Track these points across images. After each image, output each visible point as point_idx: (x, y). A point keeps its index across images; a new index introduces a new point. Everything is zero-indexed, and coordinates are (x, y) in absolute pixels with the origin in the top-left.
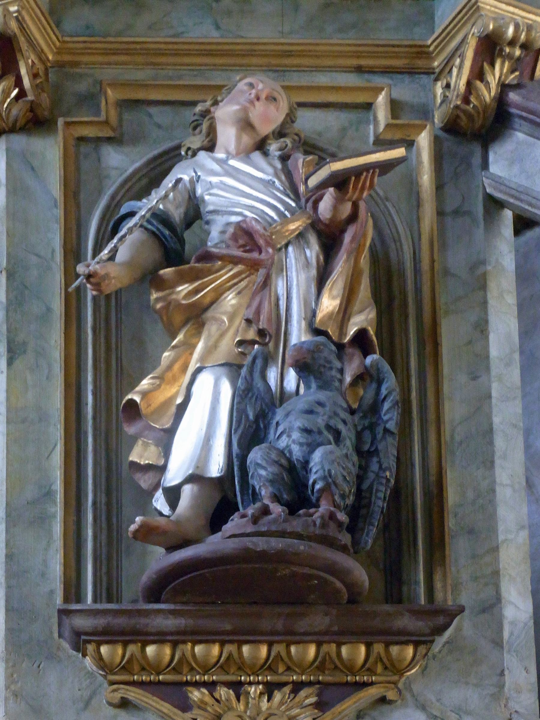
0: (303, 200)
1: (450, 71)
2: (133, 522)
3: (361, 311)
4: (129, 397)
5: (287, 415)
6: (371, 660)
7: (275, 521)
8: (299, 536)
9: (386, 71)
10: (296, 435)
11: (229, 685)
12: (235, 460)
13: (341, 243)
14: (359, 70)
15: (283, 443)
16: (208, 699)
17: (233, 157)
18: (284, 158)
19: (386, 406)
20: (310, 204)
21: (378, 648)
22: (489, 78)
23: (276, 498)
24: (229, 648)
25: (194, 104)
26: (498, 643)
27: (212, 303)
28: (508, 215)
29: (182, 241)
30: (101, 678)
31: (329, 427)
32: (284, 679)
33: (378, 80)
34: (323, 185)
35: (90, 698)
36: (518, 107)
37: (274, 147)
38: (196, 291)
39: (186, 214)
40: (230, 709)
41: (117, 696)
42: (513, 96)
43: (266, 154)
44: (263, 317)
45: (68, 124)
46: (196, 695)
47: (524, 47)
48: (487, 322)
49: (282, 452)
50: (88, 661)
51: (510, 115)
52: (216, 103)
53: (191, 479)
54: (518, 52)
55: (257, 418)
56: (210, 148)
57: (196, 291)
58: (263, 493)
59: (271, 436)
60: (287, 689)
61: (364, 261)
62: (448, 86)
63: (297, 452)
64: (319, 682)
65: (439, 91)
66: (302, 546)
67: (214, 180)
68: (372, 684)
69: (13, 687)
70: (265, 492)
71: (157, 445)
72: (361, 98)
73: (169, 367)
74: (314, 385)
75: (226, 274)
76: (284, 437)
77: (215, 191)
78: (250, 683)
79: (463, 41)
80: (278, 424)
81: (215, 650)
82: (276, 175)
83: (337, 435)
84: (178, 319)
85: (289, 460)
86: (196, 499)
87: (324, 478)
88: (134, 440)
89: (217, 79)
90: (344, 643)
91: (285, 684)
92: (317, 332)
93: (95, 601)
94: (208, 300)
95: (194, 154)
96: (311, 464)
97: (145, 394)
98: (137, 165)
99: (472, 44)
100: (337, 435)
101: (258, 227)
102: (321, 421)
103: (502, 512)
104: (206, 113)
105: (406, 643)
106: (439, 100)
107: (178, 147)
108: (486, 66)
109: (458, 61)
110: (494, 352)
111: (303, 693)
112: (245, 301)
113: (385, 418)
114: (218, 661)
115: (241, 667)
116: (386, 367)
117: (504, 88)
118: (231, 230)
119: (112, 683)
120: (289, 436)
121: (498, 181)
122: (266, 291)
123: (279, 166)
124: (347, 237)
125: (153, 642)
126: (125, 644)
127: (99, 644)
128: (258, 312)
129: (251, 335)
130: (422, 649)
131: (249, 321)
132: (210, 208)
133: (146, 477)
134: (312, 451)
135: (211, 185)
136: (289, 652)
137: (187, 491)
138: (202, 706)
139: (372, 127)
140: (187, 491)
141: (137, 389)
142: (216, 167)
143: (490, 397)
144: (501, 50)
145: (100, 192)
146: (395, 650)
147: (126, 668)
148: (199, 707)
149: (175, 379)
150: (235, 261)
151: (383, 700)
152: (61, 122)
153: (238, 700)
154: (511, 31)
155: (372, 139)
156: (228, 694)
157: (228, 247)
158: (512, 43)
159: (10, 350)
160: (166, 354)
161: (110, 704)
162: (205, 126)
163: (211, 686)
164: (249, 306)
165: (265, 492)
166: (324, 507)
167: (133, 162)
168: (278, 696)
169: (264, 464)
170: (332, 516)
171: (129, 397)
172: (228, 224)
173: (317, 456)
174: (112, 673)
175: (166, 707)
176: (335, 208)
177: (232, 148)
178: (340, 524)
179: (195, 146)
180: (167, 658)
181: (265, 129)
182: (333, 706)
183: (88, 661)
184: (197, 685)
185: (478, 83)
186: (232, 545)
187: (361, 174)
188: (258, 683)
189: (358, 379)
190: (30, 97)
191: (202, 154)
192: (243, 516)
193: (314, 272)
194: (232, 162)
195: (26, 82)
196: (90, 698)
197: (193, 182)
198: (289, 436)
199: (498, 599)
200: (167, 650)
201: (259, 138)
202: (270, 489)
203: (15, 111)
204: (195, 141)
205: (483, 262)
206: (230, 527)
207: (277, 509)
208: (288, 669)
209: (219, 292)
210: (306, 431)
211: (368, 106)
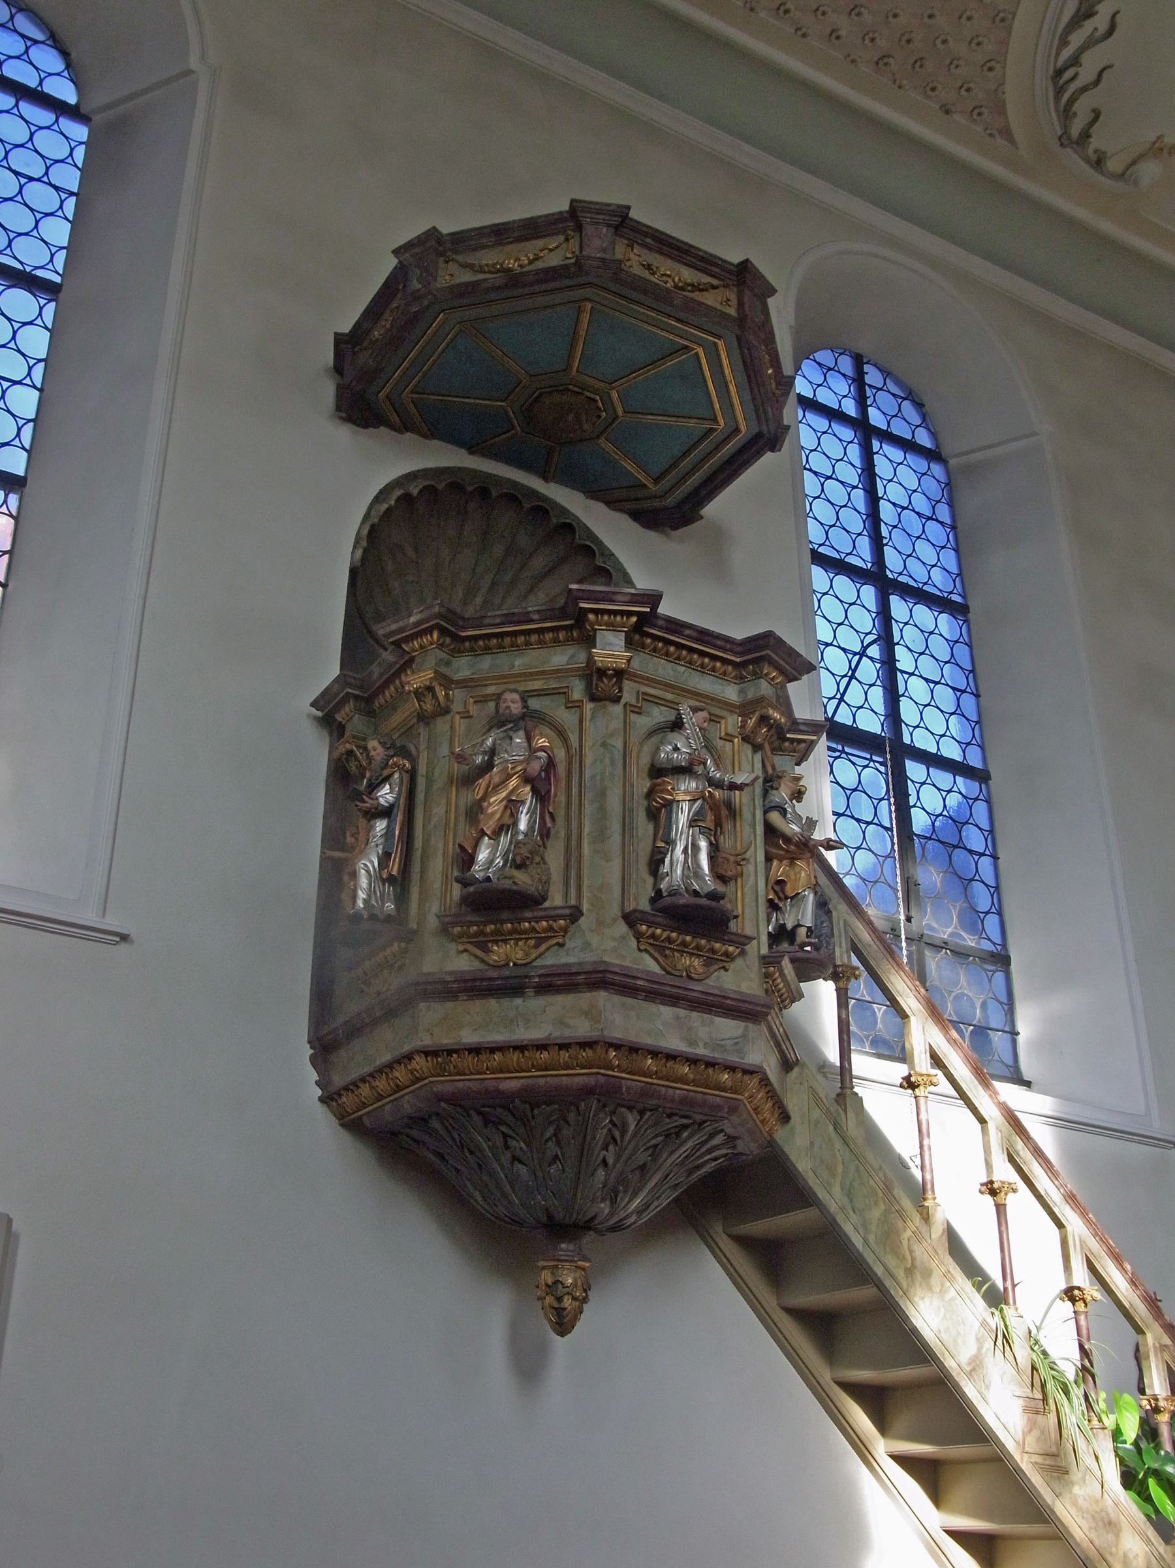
46: (667, 952)
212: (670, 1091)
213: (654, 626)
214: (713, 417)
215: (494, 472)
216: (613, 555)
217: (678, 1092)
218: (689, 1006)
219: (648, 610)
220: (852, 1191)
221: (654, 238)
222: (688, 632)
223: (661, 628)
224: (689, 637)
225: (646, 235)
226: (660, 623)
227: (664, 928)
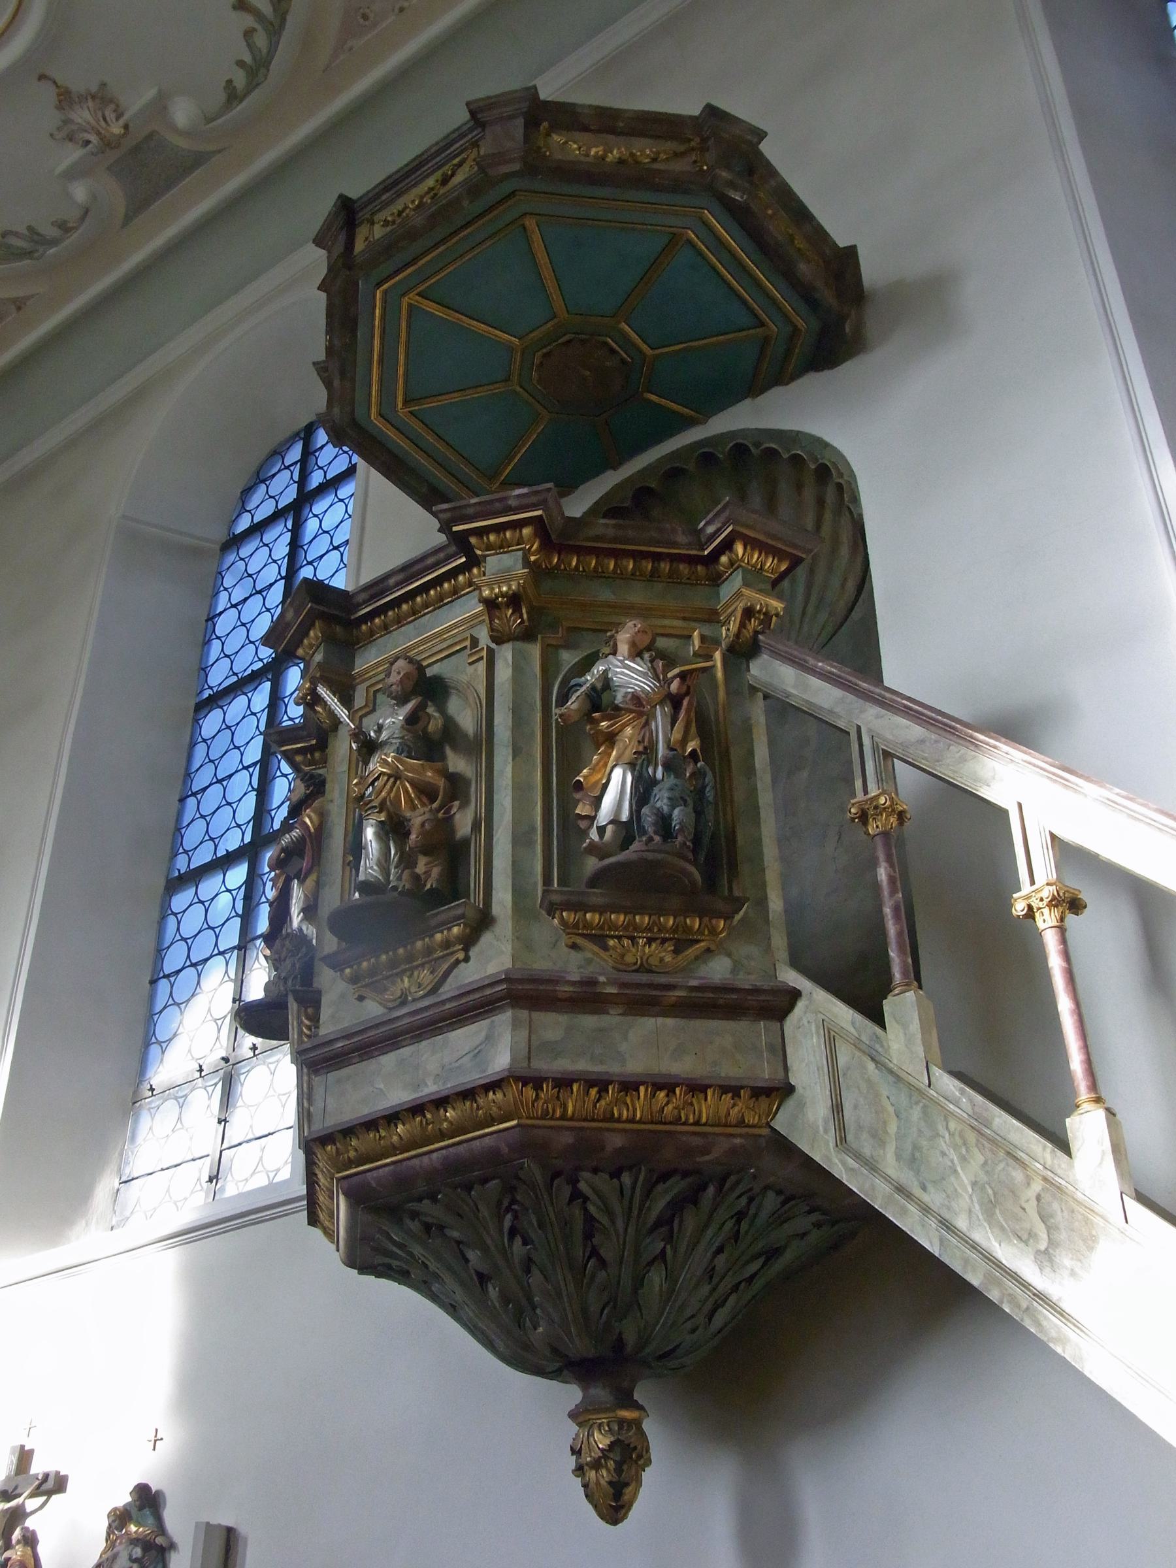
0: (662, 682)
1: (729, 623)
2: (585, 842)
3: (692, 740)
4: (577, 778)
5: (660, 791)
6: (703, 926)
7: (657, 844)
8: (668, 853)
9: (695, 620)
10: (665, 801)
11: (628, 938)
12: (634, 813)
13: (682, 705)
14: (684, 619)
15: (658, 804)
16: (618, 945)
17: (627, 660)
18: (652, 661)
19: (708, 789)
20: (666, 685)
21: (706, 920)
22: (749, 628)
23: (656, 833)
24: (630, 917)
25: (606, 631)
26: (767, 922)
27: (619, 732)
28: (760, 695)
29: (601, 698)
30: (562, 932)
31: (682, 798)
32: (657, 936)
33: (693, 624)
34: (675, 677)
35: (557, 941)
36: (764, 642)
37: (647, 656)
38: (612, 725)
39: (603, 685)
40: (629, 951)
41: (570, 942)
42: (760, 637)
43: (642, 659)
44: (646, 740)
45: (542, 638)
46: (611, 943)
47: (764, 614)
48: (753, 750)
49: (658, 809)
50: (556, 921)
51: (759, 645)
52: (617, 632)
53: (611, 822)
54: (762, 617)
55: (644, 792)
56: (614, 653)
57: (612, 725)
58: (650, 830)
59: (652, 801)
60: (658, 941)
61: (693, 714)
62: (728, 629)
63: (666, 809)
64: (675, 939)
65: (724, 632)
66: (670, 858)
67: (618, 670)
68: (703, 941)
69: (516, 934)
70: (650, 830)
71: (591, 805)
72: (686, 633)
73: (597, 764)
74: (672, 776)
75: (627, 718)
76: (659, 802)
77: (619, 676)
78: (640, 938)
79: (736, 608)
80: (655, 795)
81: (622, 917)
82: (649, 670)
83: (685, 802)
84: (601, 739)
85: (662, 814)
86: (614, 832)
87: (680, 823)
88: (578, 801)
89: (615, 619)
90: (688, 917)
91: (657, 939)
92: (672, 749)
93: (558, 886)
94: (617, 731)
95: (606, 657)
96: (674, 816)
97: (585, 777)
98: (577, 660)
99: (739, 614)
100: (685, 802)
101: (643, 696)
102: (677, 794)
103: (766, 850)
104: (612, 636)
105: (720, 917)
106: (724, 636)
107: (598, 651)
108: (747, 622)
109: (733, 618)
110: (757, 766)
111: (666, 945)
112: (637, 731)
113: (708, 795)
114: (623, 924)
115: (636, 928)
116: (707, 769)
117: (756, 633)
118: (629, 696)
119: (569, 934)
120: (662, 801)
121: (754, 677)
122: (647, 727)
123: (650, 665)
124: (685, 703)
125: (590, 911)
126: (576, 912)
127: (563, 910)
128: (643, 738)
129: (641, 749)
130: (728, 922)
131: (639, 742)
132: (617, 684)
133: (583, 822)
134: (674, 809)
135: (617, 673)
136: (660, 920)
137: (610, 828)
138: (614, 948)
139: (691, 648)
140: (610, 828)
141: (581, 774)
142: (619, 664)
143: (757, 789)
144: (754, 615)
145: (558, 673)
146: (714, 921)
147: (576, 926)
148: (613, 949)
149: (600, 770)
150: (631, 711)
151: (708, 950)
152: (539, 636)
153: (633, 946)
154: (758, 607)
155: (692, 653)
156: (628, 942)
157: (627, 704)
158: (760, 612)
159: (514, 751)
160: (595, 757)
161: (567, 946)
162: (612, 643)
163: (619, 938)
164: (639, 734)
165: (650, 830)
166: (680, 839)
167: (575, 658)
168: (654, 946)
169: (650, 814)
170: (685, 843)
171: (577, 778)
172: (627, 693)
173: (676, 812)
174: (569, 928)
175: (596, 949)
176: (679, 688)
177: (626, 654)
178: (688, 847)
179: (607, 652)
180: (597, 921)
181: (642, 647)
182: (683, 952)
183: (556, 921)
184: (612, 937)
185: (744, 630)
186: (634, 856)
187: (692, 673)
188: (644, 937)
189: (693, 775)
190: (527, 624)
191: (611, 656)
192: (640, 841)
193: (669, 720)
194: (626, 662)
195: (525, 616)
196: (557, 941)
197: (606, 672)
198: (662, 801)
199: (766, 898)
200: (597, 916)
201: (638, 650)
202: (653, 828)
203: (517, 631)
204: (607, 650)
205: (750, 718)
206: (633, 847)
207: (657, 838)
208: (659, 930)
209: (624, 726)
210: (669, 799)
211: (690, 637)
212: (426, 1159)
213: (358, 606)
214: (672, 235)
215: (630, 473)
216: (798, 432)
217: (435, 1155)
218: (412, 1037)
219: (464, 559)
220: (917, 1155)
221: (386, 189)
222: (392, 581)
223: (366, 602)
224: (400, 584)
225: (378, 196)
226: (361, 598)
227: (600, 910)
